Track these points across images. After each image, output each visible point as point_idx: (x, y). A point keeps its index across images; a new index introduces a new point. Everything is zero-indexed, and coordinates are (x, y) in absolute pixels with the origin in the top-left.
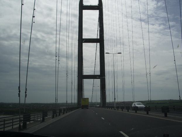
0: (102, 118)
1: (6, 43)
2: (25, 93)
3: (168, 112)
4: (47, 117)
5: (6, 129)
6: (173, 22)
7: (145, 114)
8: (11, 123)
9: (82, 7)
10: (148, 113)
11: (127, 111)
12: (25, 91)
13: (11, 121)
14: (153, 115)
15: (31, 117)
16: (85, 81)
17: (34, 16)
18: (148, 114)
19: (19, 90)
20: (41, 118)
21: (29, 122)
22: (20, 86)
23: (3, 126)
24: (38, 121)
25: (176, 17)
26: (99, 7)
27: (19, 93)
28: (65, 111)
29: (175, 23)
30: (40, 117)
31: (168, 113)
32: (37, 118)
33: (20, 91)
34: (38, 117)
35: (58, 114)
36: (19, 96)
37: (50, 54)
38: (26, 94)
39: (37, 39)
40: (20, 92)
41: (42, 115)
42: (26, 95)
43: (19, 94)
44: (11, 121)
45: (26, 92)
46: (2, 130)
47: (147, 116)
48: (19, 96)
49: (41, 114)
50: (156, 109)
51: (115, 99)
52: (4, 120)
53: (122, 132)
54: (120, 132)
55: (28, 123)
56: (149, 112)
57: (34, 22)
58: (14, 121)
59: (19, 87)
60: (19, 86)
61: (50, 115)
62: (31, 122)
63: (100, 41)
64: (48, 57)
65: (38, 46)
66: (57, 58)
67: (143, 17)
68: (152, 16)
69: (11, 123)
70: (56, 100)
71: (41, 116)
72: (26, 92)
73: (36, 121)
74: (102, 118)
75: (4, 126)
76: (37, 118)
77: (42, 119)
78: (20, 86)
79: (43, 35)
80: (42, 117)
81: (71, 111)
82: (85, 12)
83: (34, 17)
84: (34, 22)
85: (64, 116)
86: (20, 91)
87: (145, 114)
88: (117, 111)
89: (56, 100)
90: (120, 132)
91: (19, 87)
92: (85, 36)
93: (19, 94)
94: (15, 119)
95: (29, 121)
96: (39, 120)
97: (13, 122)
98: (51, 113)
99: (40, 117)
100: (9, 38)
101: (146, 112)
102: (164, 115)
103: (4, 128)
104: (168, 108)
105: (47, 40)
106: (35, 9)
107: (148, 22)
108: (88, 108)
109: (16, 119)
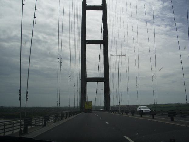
0: (106, 122)
1: (6, 45)
2: (26, 97)
3: (174, 116)
4: (48, 122)
5: (7, 134)
6: (179, 22)
7: (150, 118)
8: (11, 127)
9: (85, 8)
10: (154, 117)
11: (132, 115)
12: (26, 94)
13: (12, 126)
14: (158, 119)
15: (32, 121)
16: (89, 84)
17: (35, 16)
18: (153, 118)
19: (19, 93)
20: (42, 122)
21: (30, 126)
22: (20, 89)
23: (3, 130)
24: (39, 125)
25: (183, 18)
26: (103, 8)
27: (19, 96)
28: (68, 115)
29: (181, 24)
30: (41, 121)
31: (174, 117)
32: (38, 122)
33: (20, 95)
34: (40, 122)
35: (60, 118)
36: (20, 100)
37: (52, 56)
38: (27, 97)
39: (38, 41)
40: (21, 96)
41: (43, 119)
42: (27, 99)
43: (20, 98)
44: (12, 126)
45: (27, 96)
46: (2, 135)
47: (153, 120)
48: (20, 100)
49: (42, 118)
50: (162, 113)
51: (119, 103)
52: (4, 124)
53: (126, 137)
54: (125, 137)
55: (29, 127)
56: (155, 116)
57: (35, 23)
58: (15, 125)
59: (20, 90)
60: (20, 89)
61: (52, 119)
62: (32, 126)
63: (104, 42)
64: (50, 59)
65: (39, 47)
66: (59, 60)
67: (149, 17)
68: (157, 17)
69: (11, 127)
70: (59, 104)
71: (42, 120)
72: (27, 96)
73: (37, 125)
74: (106, 122)
75: (4, 131)
76: (38, 122)
77: (43, 123)
78: (20, 89)
79: (45, 36)
80: (43, 121)
81: (74, 115)
82: (88, 12)
83: (36, 17)
84: (35, 23)
85: (66, 120)
86: (20, 95)
87: (150, 118)
88: (122, 115)
89: (58, 103)
90: (125, 137)
91: (20, 90)
92: (88, 37)
93: (20, 98)
94: (15, 123)
95: (30, 125)
96: (41, 124)
97: (13, 127)
98: (53, 117)
99: (41, 121)
100: (9, 39)
101: (152, 116)
102: (170, 119)
103: (4, 132)
104: (175, 112)
105: (49, 41)
106: (36, 10)
107: (153, 23)
108: (91, 112)
109: (16, 123)
